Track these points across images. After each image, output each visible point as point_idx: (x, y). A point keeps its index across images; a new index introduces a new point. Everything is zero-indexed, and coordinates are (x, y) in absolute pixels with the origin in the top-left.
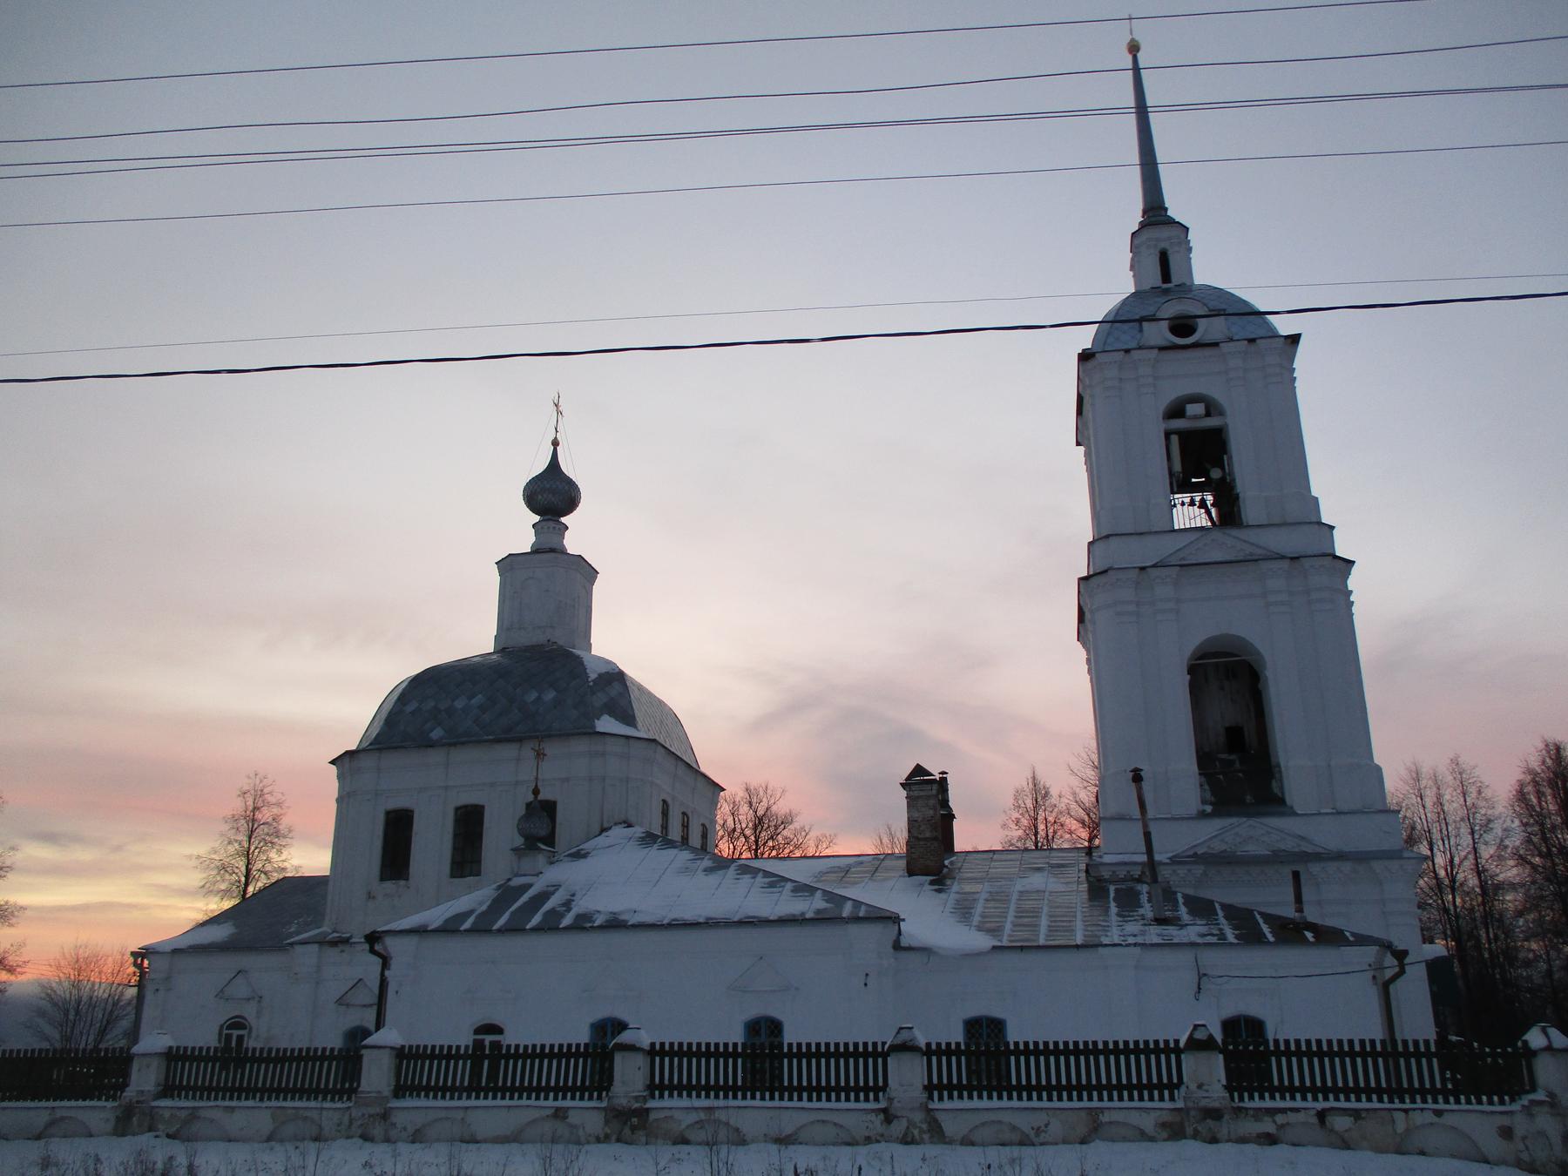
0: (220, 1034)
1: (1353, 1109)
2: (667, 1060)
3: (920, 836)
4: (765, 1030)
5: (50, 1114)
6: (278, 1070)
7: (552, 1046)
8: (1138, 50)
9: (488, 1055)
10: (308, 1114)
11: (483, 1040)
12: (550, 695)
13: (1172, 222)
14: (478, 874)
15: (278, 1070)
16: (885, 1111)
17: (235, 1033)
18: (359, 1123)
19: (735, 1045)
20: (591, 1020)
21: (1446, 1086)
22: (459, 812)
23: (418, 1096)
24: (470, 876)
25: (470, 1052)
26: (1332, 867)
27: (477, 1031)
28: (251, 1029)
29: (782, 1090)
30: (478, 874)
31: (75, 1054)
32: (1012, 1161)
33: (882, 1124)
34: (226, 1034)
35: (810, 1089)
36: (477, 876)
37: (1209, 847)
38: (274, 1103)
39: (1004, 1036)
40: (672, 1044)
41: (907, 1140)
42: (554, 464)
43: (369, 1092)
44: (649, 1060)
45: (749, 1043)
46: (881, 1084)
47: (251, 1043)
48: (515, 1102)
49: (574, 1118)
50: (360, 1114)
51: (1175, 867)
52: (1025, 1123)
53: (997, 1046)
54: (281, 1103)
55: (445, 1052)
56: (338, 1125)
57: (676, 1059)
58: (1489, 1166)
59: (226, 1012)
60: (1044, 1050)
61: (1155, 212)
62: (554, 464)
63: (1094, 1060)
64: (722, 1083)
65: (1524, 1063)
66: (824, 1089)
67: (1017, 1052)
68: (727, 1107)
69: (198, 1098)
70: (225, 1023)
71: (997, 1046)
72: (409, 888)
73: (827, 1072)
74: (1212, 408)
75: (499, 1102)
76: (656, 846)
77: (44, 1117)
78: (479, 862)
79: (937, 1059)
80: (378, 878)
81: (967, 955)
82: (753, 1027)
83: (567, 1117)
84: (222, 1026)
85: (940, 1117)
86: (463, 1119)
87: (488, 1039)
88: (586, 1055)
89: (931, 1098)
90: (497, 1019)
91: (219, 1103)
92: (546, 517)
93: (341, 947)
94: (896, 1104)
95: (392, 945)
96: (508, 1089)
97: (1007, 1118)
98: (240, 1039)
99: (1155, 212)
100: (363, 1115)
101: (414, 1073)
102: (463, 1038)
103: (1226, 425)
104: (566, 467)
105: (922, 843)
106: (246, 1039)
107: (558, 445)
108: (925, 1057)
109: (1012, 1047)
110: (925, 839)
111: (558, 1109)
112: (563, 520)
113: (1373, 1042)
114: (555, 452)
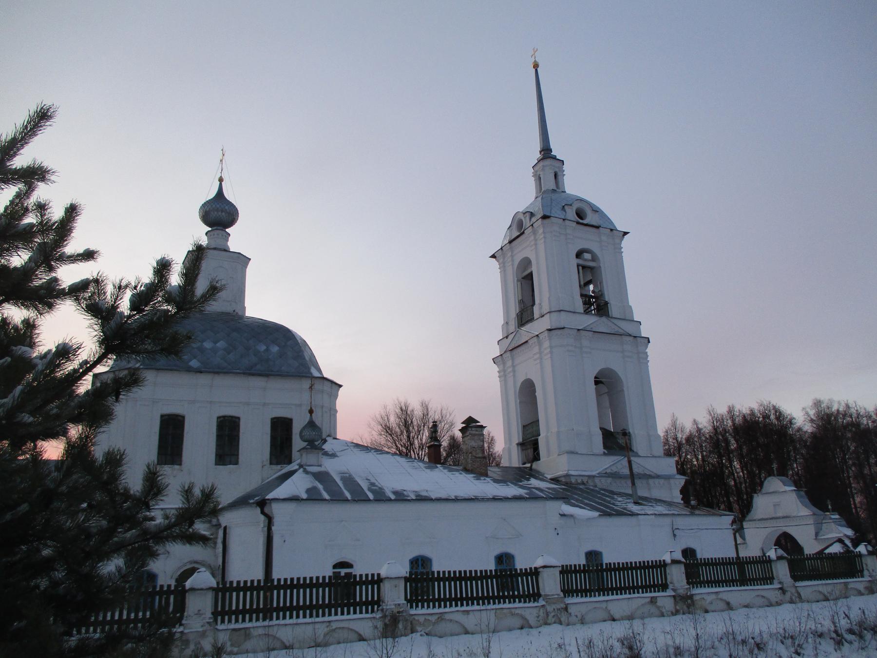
2: (314, 590)
3: (477, 456)
4: (593, 556)
5: (327, 627)
7: (252, 581)
10: (517, 611)
11: (340, 572)
12: (275, 349)
13: (554, 158)
14: (236, 463)
16: (781, 589)
18: (553, 614)
19: (259, 581)
20: (409, 558)
21: (505, 594)
23: (573, 596)
25: (262, 584)
26: (657, 481)
27: (335, 567)
29: (355, 604)
30: (236, 463)
31: (601, 567)
33: (780, 595)
35: (467, 599)
36: (236, 465)
37: (611, 470)
38: (497, 606)
39: (514, 565)
41: (792, 602)
42: (220, 194)
43: (553, 595)
44: (214, 594)
45: (413, 572)
48: (633, 596)
49: (660, 602)
50: (552, 609)
51: (600, 478)
52: (825, 590)
54: (501, 606)
55: (370, 579)
56: (538, 617)
58: (365, 642)
61: (546, 152)
62: (220, 194)
63: (459, 583)
64: (448, 596)
67: (439, 579)
68: (486, 609)
72: (182, 471)
74: (594, 258)
75: (624, 596)
77: (321, 630)
78: (238, 455)
80: (213, 457)
81: (589, 519)
83: (656, 602)
85: (800, 590)
86: (606, 607)
87: (343, 572)
88: (329, 585)
89: (216, 621)
90: (348, 558)
91: (459, 608)
92: (214, 228)
94: (785, 585)
95: (277, 510)
97: (821, 589)
99: (546, 152)
100: (554, 609)
101: (765, 570)
102: (327, 571)
104: (228, 195)
105: (478, 459)
107: (223, 181)
109: (519, 572)
110: (479, 458)
111: (652, 598)
112: (227, 230)
113: (580, 565)
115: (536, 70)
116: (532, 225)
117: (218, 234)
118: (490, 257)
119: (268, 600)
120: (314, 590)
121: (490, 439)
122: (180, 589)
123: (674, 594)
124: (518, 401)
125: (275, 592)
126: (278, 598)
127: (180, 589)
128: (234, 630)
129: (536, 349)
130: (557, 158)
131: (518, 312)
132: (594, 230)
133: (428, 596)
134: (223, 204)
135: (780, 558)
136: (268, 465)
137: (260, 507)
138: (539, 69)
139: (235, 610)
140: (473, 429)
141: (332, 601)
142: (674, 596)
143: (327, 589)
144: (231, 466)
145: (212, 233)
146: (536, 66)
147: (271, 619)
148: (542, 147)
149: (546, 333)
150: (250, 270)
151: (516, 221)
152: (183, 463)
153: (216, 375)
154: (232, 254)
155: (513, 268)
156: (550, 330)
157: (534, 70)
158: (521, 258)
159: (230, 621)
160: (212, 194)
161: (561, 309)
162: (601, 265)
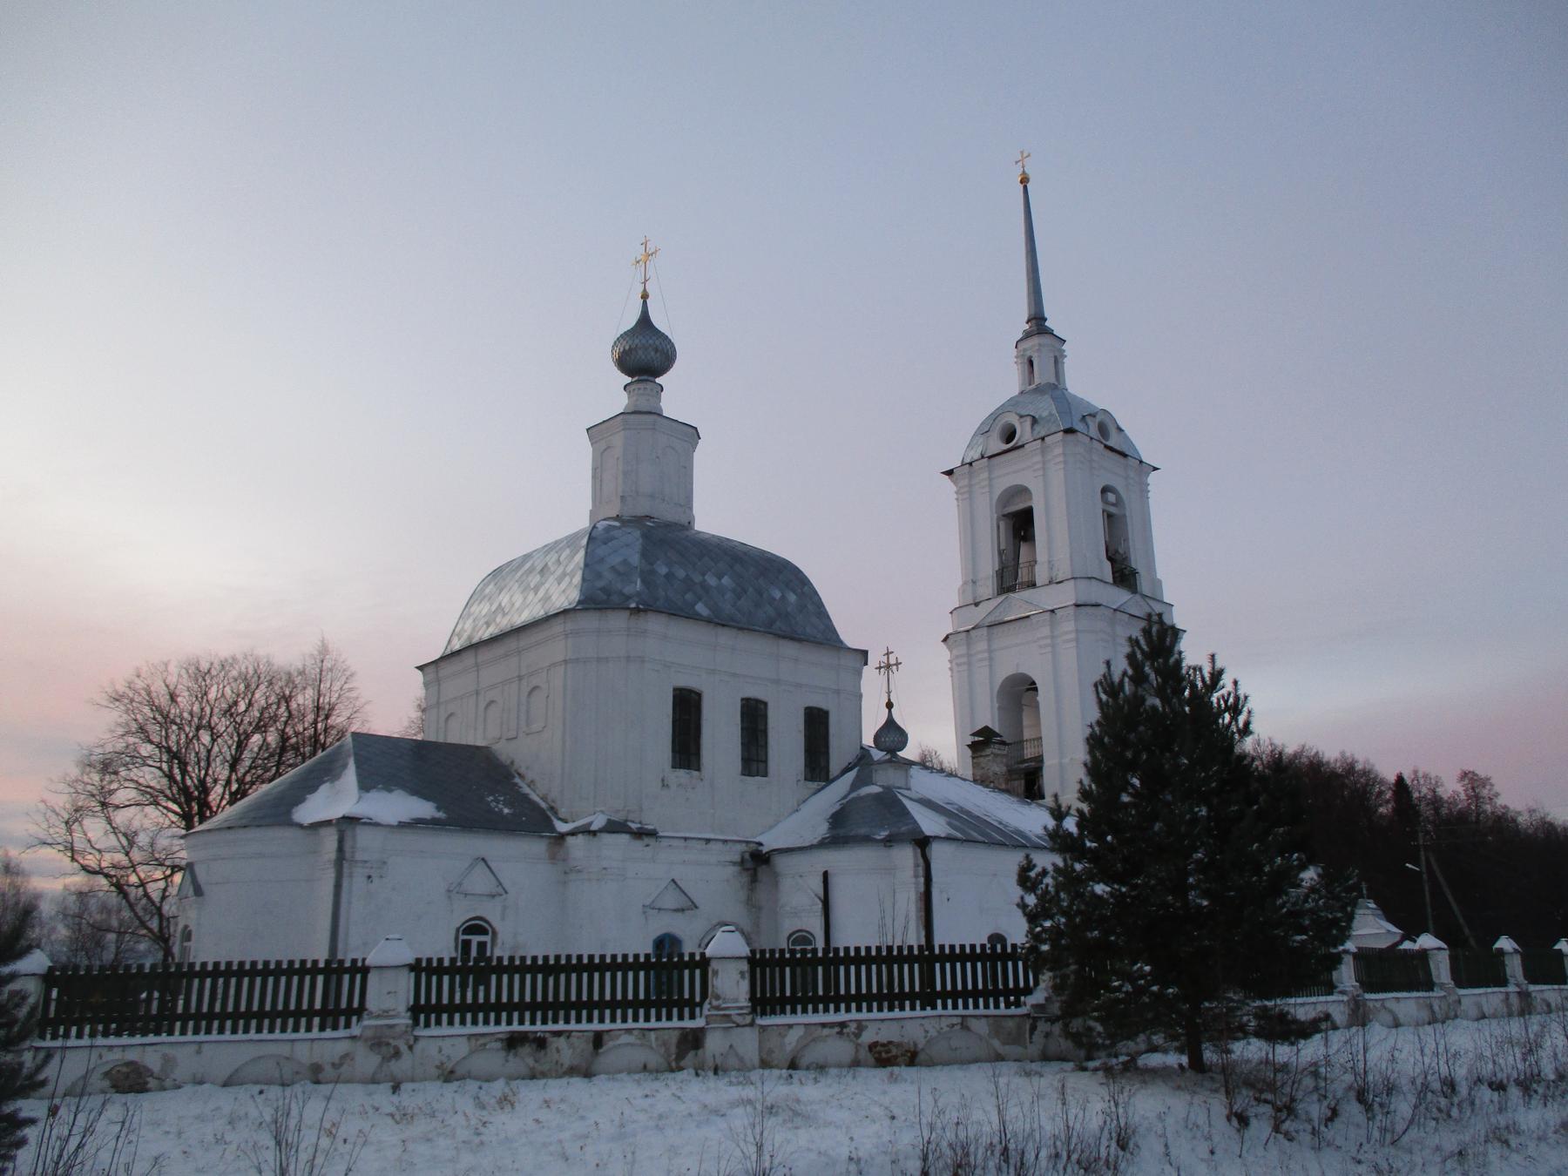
0: (457, 938)
1: (373, 1026)
2: (505, 978)
6: (777, 975)
8: (1028, 181)
9: (346, 973)
13: (1050, 332)
14: (765, 775)
15: (777, 975)
17: (475, 939)
22: (762, 707)
24: (757, 775)
28: (494, 933)
30: (765, 775)
31: (834, 954)
32: (261, 1092)
34: (463, 941)
40: (868, 949)
42: (645, 321)
46: (356, 1004)
47: (501, 951)
53: (670, 957)
54: (481, 1029)
57: (874, 967)
59: (461, 916)
60: (840, 965)
61: (1038, 323)
62: (645, 321)
65: (1108, 963)
66: (304, 1014)
69: (778, 1012)
70: (461, 926)
71: (670, 957)
73: (247, 995)
76: (1086, 781)
78: (765, 762)
79: (972, 965)
80: (737, 765)
82: (660, 943)
84: (458, 930)
92: (636, 378)
93: (647, 840)
96: (227, 1016)
98: (482, 946)
99: (1038, 323)
103: (1125, 516)
104: (658, 321)
106: (489, 946)
108: (413, 974)
112: (657, 380)
114: (645, 303)
115: (1025, 188)
116: (1043, 439)
117: (652, 390)
118: (943, 473)
119: (928, 979)
120: (631, 975)
121: (143, 693)
122: (482, 964)
123: (1518, 990)
124: (997, 705)
125: (687, 972)
126: (942, 978)
127: (482, 964)
128: (470, 1036)
129: (1046, 631)
130: (1055, 333)
131: (997, 569)
132: (1117, 457)
133: (670, 994)
134: (644, 337)
135: (1516, 951)
136: (803, 781)
137: (919, 847)
138: (1029, 186)
139: (233, 1012)
140: (997, 746)
141: (652, 994)
142: (1519, 993)
143: (642, 974)
144: (759, 778)
145: (633, 387)
146: (1025, 180)
147: (171, 1033)
148: (1033, 313)
149: (1071, 610)
150: (702, 457)
151: (998, 428)
152: (703, 768)
153: (740, 632)
154: (665, 420)
155: (991, 500)
156: (1077, 606)
157: (1021, 187)
158: (1020, 483)
159: (463, 1022)
160: (631, 320)
161: (1094, 576)
162: (1127, 514)
